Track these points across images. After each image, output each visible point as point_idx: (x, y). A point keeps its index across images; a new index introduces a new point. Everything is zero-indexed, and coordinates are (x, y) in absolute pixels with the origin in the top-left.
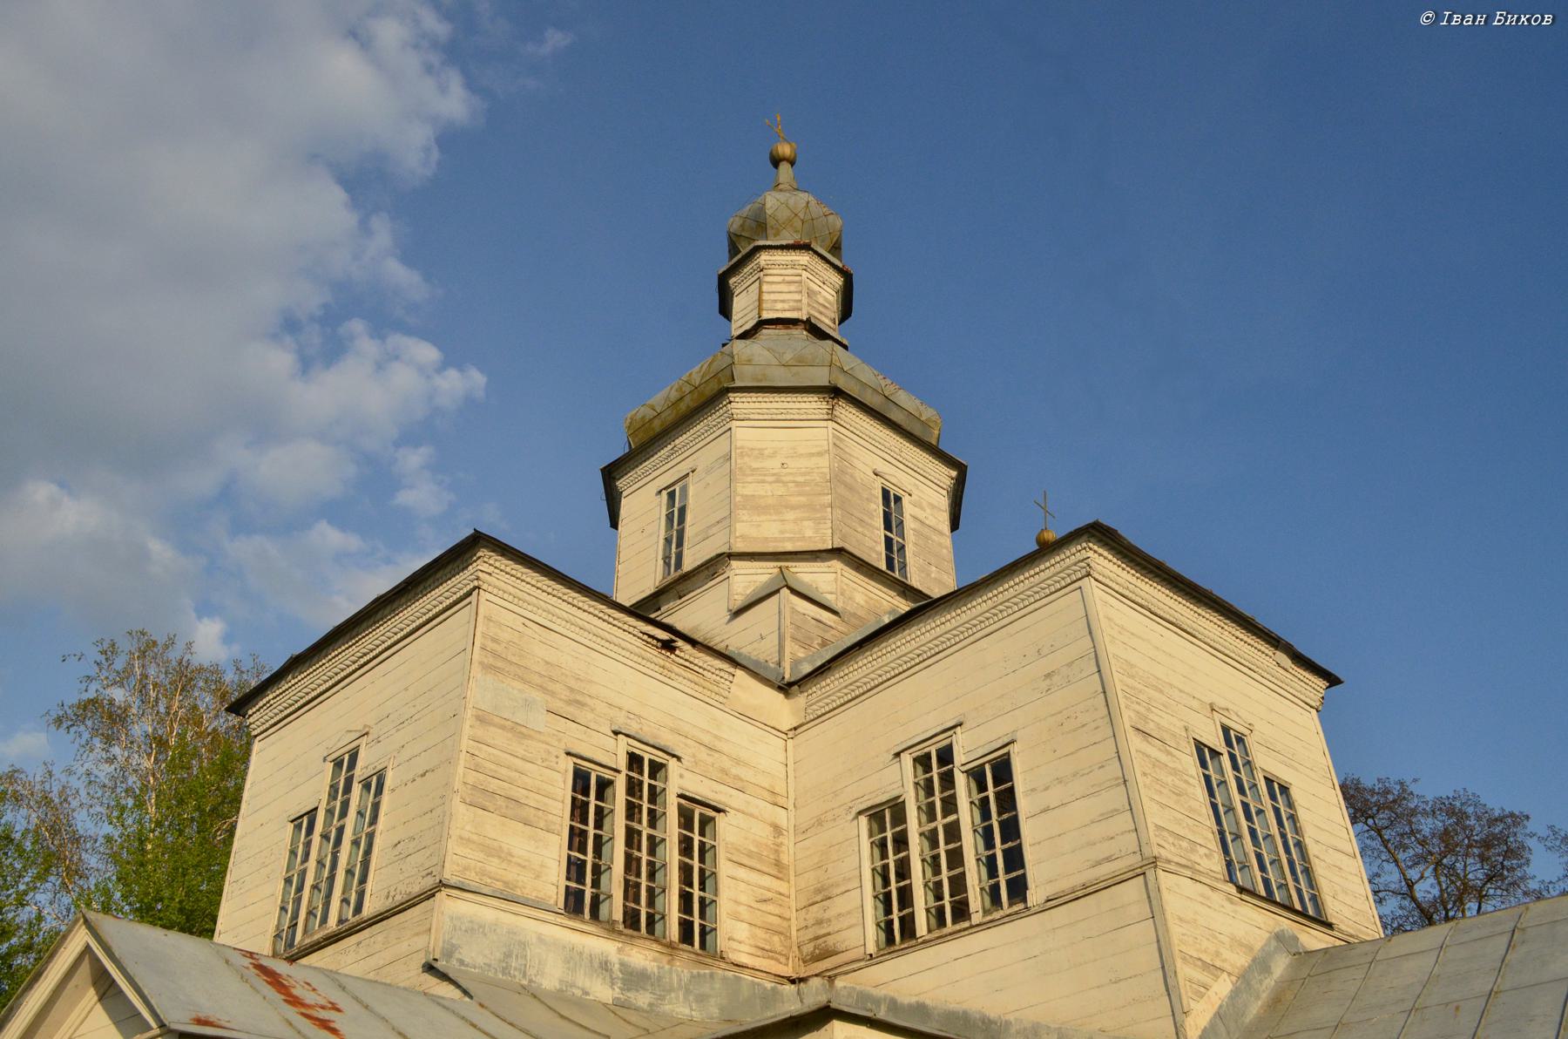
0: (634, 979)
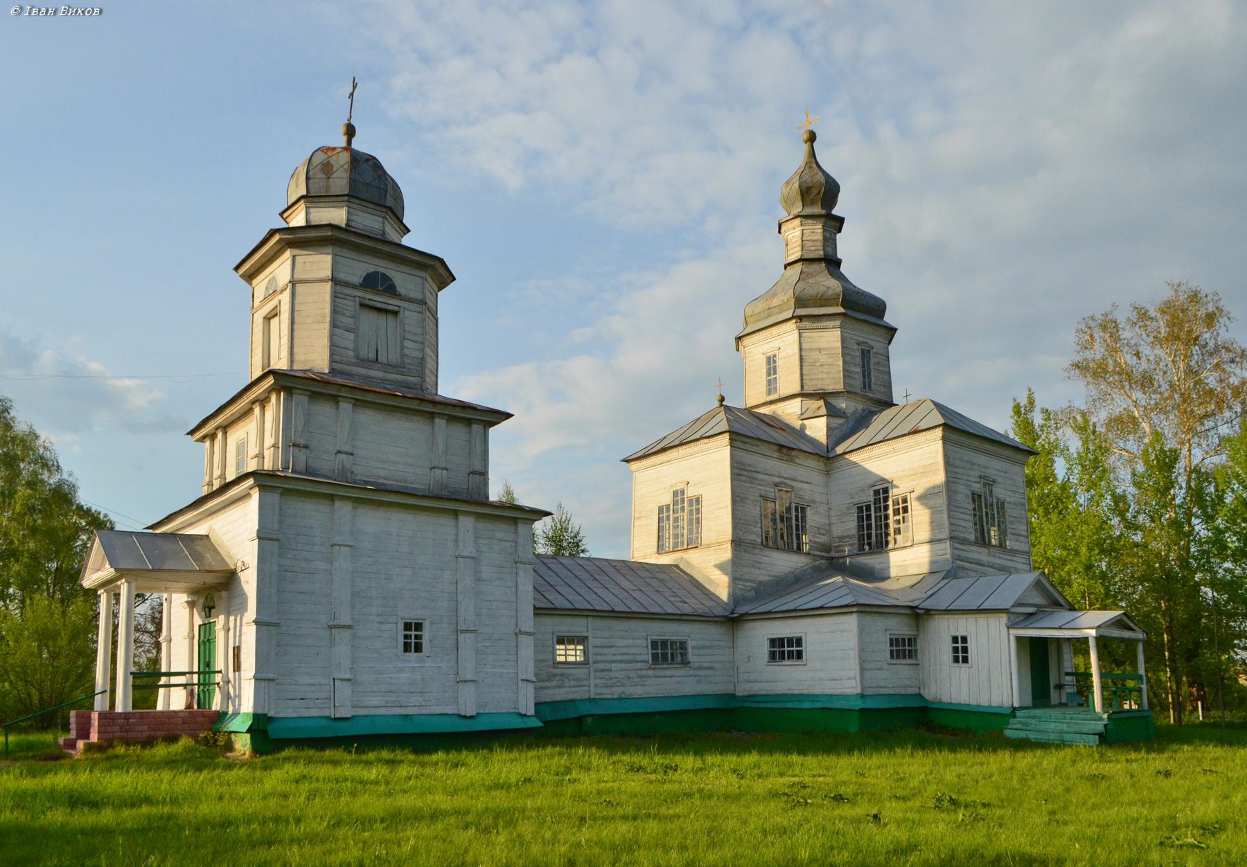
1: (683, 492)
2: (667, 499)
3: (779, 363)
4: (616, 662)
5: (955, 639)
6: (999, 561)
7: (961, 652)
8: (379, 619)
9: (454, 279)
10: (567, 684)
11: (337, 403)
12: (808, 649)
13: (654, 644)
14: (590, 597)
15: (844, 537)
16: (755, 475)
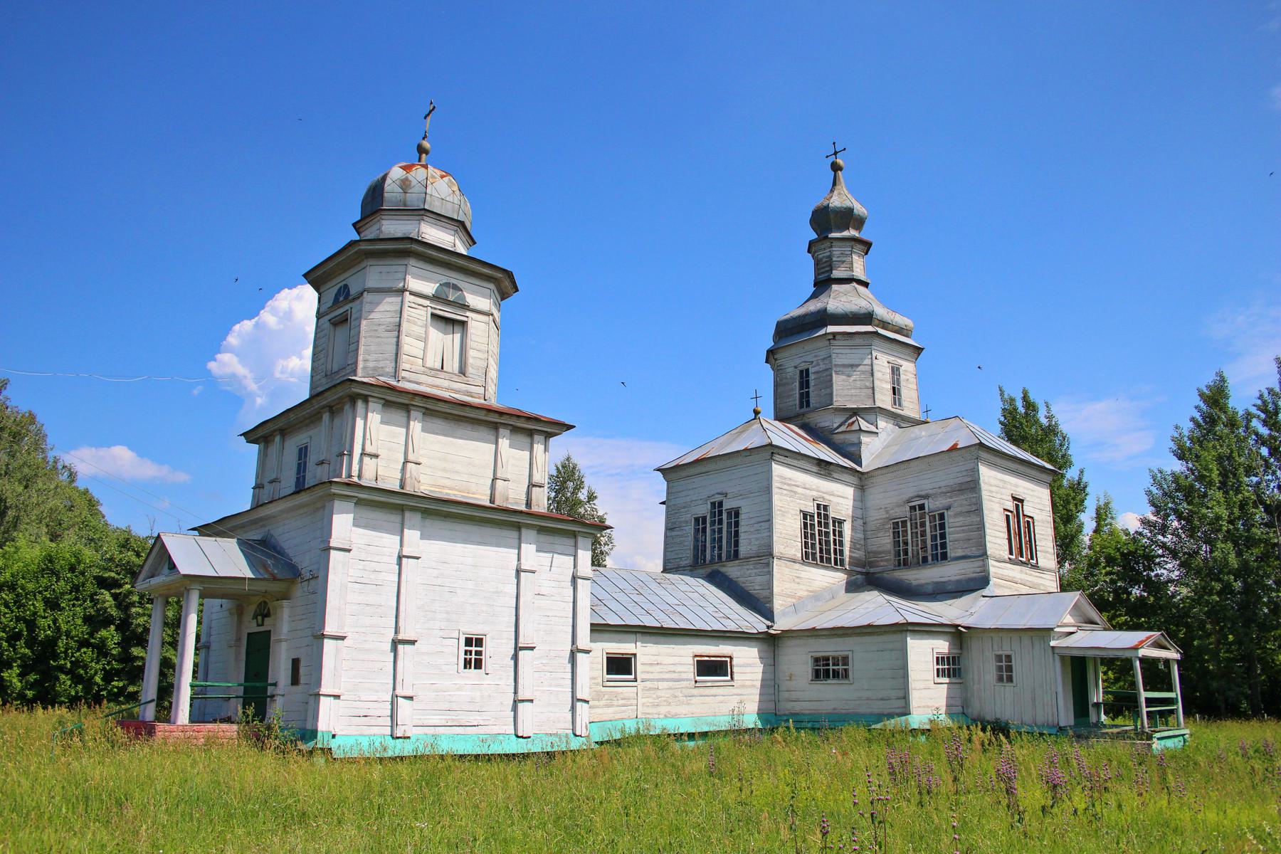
1: (721, 504)
2: (704, 510)
3: (812, 377)
4: (663, 680)
5: (999, 658)
6: (1029, 578)
7: (1006, 672)
8: (441, 633)
9: (517, 290)
10: (615, 703)
11: (408, 412)
12: (640, 667)
13: (817, 660)
14: (662, 617)
15: (880, 553)
16: (795, 489)
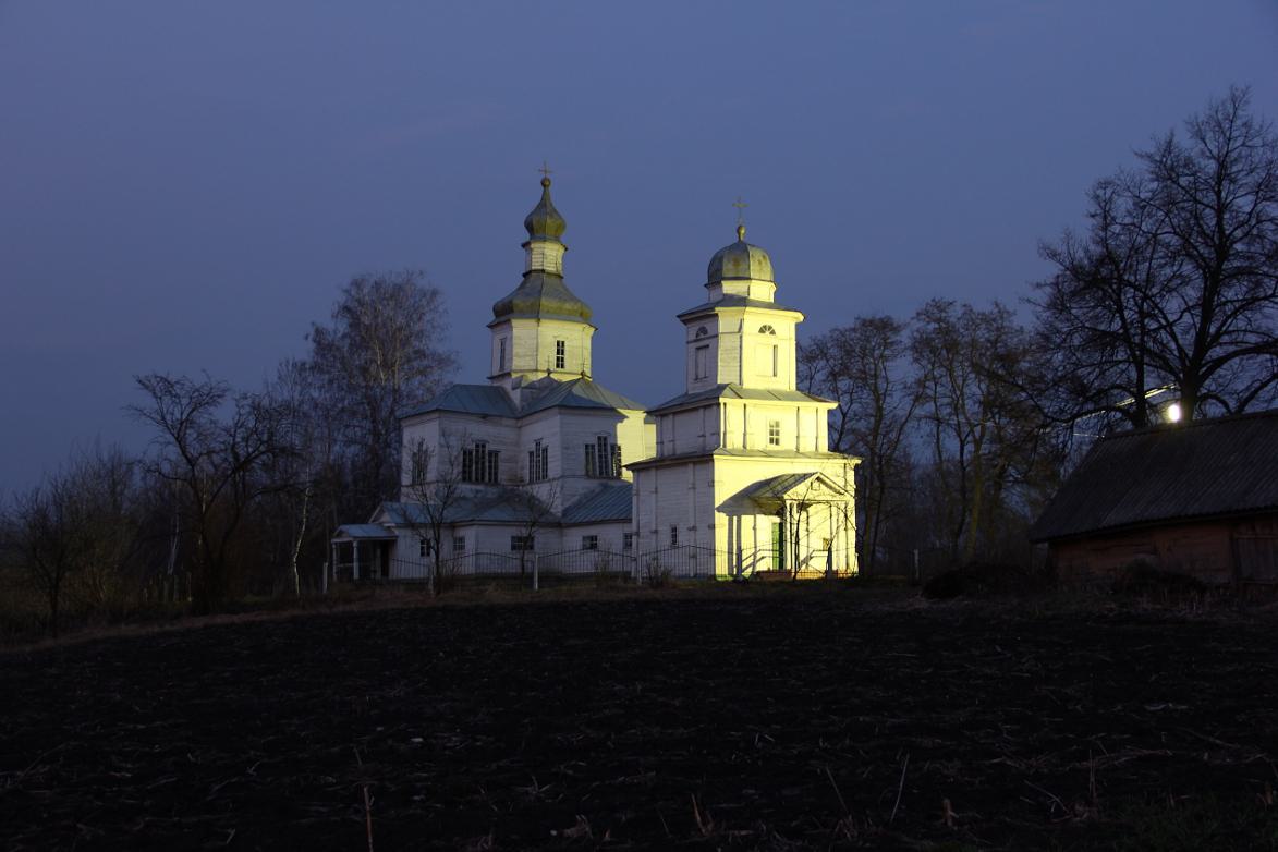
0: (477, 492)
3: (566, 348)
